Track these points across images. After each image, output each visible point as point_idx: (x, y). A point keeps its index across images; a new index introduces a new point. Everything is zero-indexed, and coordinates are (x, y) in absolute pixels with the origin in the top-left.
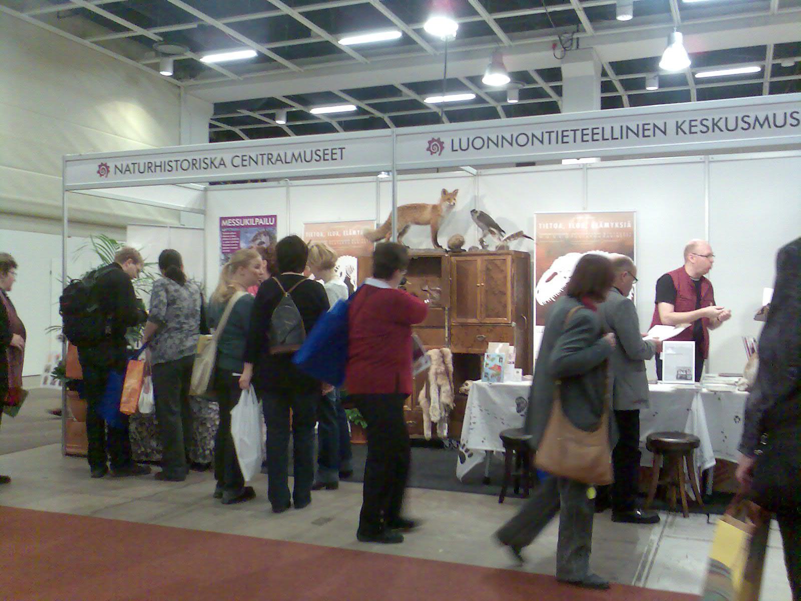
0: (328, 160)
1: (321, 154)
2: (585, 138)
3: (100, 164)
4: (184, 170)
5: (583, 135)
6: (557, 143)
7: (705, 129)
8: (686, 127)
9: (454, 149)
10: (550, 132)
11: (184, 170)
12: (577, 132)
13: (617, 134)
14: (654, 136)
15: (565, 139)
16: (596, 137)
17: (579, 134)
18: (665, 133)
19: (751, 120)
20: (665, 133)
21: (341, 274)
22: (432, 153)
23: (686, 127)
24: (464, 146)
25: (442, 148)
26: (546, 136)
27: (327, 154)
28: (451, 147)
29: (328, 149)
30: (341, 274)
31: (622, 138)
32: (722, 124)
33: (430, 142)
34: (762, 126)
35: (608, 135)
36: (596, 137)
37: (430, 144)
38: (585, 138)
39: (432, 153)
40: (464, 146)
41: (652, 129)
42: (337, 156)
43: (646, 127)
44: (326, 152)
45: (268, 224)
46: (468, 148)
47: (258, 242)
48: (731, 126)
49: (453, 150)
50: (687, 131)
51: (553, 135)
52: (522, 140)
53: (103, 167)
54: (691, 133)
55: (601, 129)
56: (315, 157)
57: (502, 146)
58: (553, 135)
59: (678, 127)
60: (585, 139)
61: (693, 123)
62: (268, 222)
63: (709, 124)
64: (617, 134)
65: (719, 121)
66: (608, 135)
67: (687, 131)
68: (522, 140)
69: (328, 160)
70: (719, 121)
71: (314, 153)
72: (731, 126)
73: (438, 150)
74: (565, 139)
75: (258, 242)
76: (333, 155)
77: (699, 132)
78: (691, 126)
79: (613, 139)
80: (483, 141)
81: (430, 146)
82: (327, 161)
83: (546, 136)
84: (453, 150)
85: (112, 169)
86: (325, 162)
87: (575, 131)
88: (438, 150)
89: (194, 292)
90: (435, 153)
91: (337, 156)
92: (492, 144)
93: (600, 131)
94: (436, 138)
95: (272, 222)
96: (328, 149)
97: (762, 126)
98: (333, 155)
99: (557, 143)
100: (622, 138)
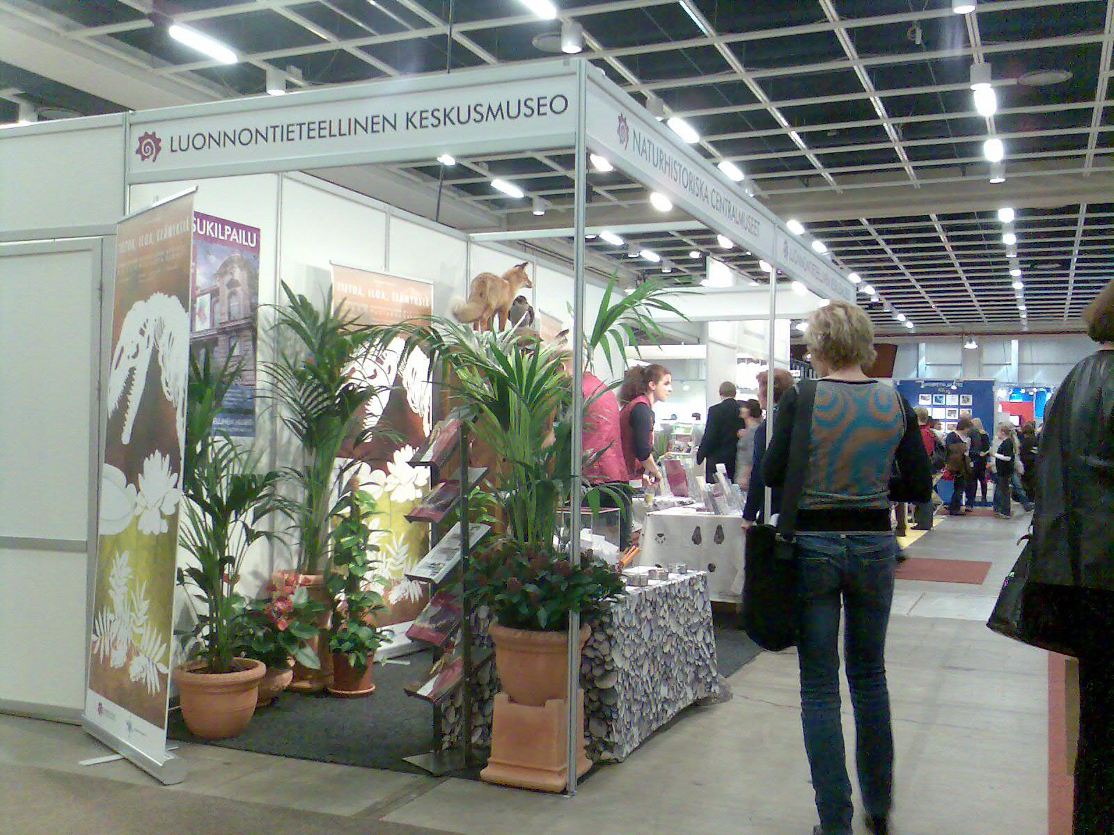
0: (378, 132)
1: (534, 105)
2: (312, 133)
3: (142, 134)
4: (197, 149)
5: (309, 130)
6: (282, 140)
7: (436, 122)
8: (416, 120)
9: (342, 132)
10: (274, 127)
11: (197, 149)
12: (277, 129)
13: (345, 130)
14: (384, 131)
15: (291, 136)
16: (322, 133)
17: (305, 128)
18: (394, 127)
19: (484, 110)
20: (394, 127)
21: (389, 368)
22: (144, 158)
23: (416, 120)
24: (184, 146)
25: (158, 149)
26: (271, 131)
27: (325, 128)
28: (170, 146)
29: (314, 123)
30: (389, 368)
31: (350, 134)
32: (453, 116)
33: (141, 140)
34: (495, 117)
35: (335, 131)
36: (322, 133)
37: (141, 143)
38: (312, 133)
39: (144, 158)
40: (184, 146)
41: (381, 123)
42: (295, 135)
43: (375, 120)
44: (323, 125)
45: (244, 243)
46: (202, 147)
47: (227, 278)
48: (463, 117)
49: (172, 151)
50: (418, 125)
51: (278, 131)
52: (245, 137)
53: (149, 140)
54: (421, 126)
55: (328, 123)
56: (524, 110)
57: (355, 133)
58: (278, 131)
59: (409, 120)
60: (311, 135)
61: (424, 115)
62: (247, 240)
63: (441, 115)
64: (345, 130)
65: (451, 111)
66: (335, 131)
67: (418, 125)
68: (245, 137)
69: (378, 132)
70: (451, 111)
71: (472, 110)
72: (463, 117)
73: (152, 153)
74: (291, 136)
75: (227, 278)
76: (321, 131)
77: (430, 126)
78: (421, 118)
79: (340, 134)
80: (250, 132)
81: (141, 145)
82: (344, 137)
83: (271, 131)
84: (172, 151)
85: (165, 145)
86: (375, 134)
87: (301, 125)
88: (152, 153)
89: (1005, 438)
90: (148, 157)
91: (295, 135)
92: (389, 125)
93: (327, 125)
94: (150, 133)
95: (252, 242)
96: (314, 123)
97: (495, 117)
98: (321, 131)
99: (282, 140)
100: (350, 134)
